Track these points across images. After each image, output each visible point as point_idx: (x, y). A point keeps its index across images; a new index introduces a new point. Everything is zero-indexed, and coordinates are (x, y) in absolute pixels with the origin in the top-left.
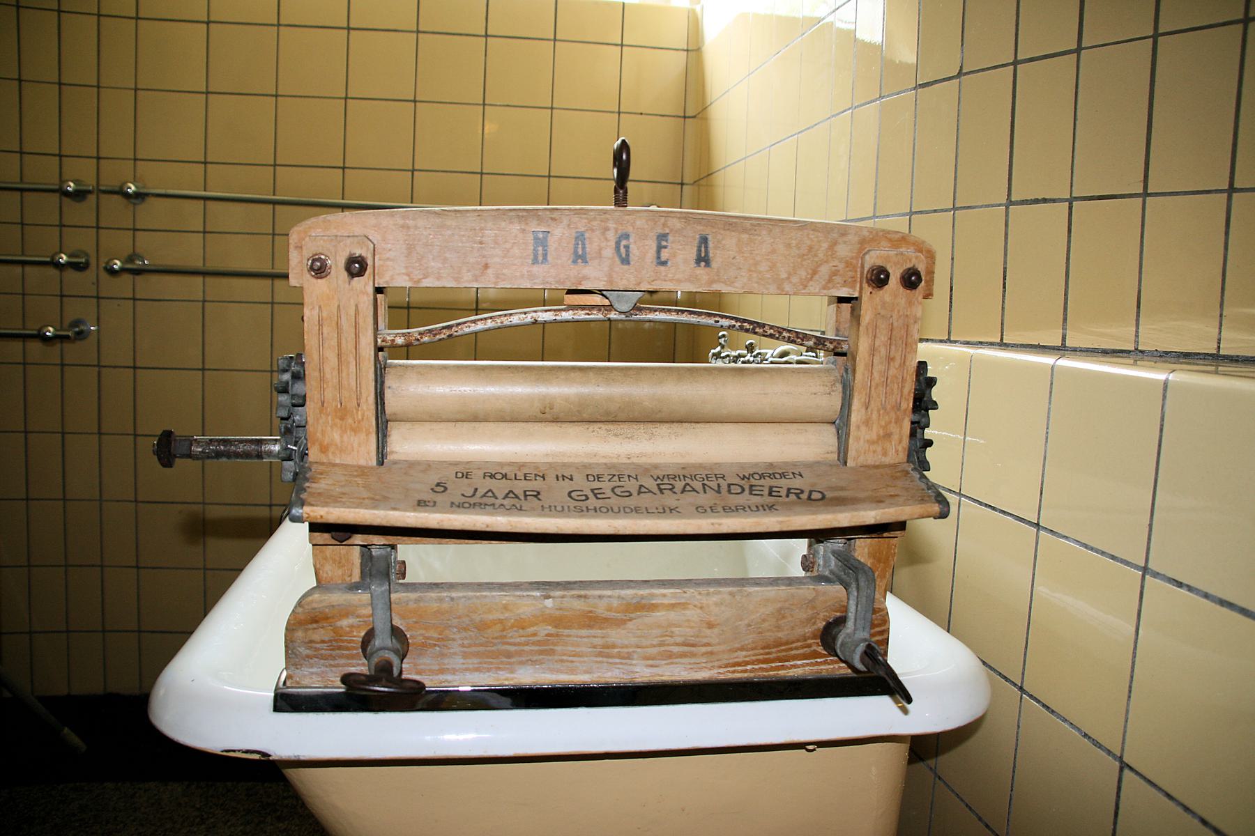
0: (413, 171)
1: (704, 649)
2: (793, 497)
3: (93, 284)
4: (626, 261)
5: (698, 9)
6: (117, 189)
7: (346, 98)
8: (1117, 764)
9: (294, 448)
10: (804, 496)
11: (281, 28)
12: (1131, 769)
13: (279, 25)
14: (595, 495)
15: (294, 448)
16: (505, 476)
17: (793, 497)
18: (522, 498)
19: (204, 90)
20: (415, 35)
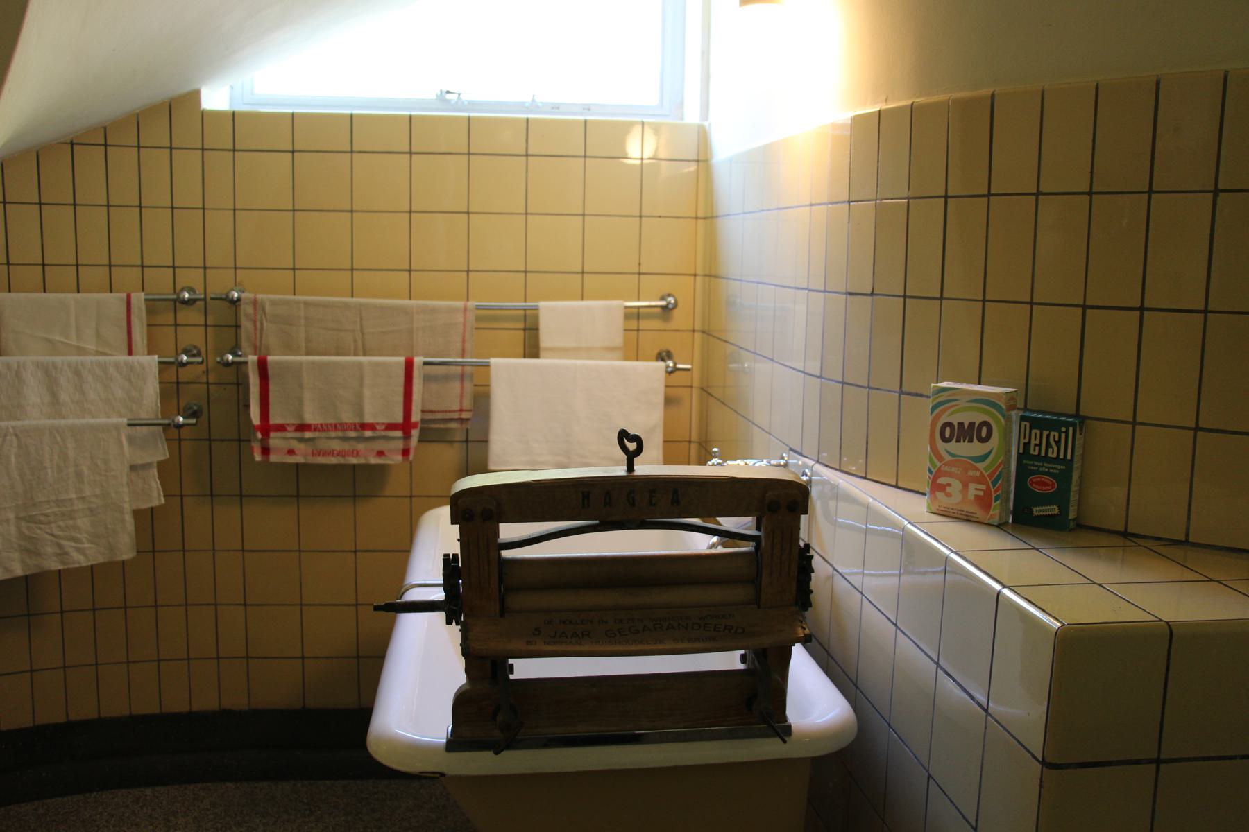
0: (468, 271)
1: (963, 513)
2: (727, 631)
3: (204, 372)
4: (633, 504)
5: (706, 124)
6: (224, 296)
7: (410, 212)
8: (927, 774)
9: (455, 608)
10: (733, 631)
11: (354, 155)
12: (933, 779)
13: (352, 152)
14: (620, 633)
15: (455, 608)
16: (571, 622)
17: (727, 631)
18: (581, 636)
19: (291, 208)
20: (466, 157)
